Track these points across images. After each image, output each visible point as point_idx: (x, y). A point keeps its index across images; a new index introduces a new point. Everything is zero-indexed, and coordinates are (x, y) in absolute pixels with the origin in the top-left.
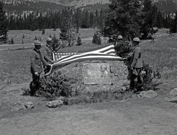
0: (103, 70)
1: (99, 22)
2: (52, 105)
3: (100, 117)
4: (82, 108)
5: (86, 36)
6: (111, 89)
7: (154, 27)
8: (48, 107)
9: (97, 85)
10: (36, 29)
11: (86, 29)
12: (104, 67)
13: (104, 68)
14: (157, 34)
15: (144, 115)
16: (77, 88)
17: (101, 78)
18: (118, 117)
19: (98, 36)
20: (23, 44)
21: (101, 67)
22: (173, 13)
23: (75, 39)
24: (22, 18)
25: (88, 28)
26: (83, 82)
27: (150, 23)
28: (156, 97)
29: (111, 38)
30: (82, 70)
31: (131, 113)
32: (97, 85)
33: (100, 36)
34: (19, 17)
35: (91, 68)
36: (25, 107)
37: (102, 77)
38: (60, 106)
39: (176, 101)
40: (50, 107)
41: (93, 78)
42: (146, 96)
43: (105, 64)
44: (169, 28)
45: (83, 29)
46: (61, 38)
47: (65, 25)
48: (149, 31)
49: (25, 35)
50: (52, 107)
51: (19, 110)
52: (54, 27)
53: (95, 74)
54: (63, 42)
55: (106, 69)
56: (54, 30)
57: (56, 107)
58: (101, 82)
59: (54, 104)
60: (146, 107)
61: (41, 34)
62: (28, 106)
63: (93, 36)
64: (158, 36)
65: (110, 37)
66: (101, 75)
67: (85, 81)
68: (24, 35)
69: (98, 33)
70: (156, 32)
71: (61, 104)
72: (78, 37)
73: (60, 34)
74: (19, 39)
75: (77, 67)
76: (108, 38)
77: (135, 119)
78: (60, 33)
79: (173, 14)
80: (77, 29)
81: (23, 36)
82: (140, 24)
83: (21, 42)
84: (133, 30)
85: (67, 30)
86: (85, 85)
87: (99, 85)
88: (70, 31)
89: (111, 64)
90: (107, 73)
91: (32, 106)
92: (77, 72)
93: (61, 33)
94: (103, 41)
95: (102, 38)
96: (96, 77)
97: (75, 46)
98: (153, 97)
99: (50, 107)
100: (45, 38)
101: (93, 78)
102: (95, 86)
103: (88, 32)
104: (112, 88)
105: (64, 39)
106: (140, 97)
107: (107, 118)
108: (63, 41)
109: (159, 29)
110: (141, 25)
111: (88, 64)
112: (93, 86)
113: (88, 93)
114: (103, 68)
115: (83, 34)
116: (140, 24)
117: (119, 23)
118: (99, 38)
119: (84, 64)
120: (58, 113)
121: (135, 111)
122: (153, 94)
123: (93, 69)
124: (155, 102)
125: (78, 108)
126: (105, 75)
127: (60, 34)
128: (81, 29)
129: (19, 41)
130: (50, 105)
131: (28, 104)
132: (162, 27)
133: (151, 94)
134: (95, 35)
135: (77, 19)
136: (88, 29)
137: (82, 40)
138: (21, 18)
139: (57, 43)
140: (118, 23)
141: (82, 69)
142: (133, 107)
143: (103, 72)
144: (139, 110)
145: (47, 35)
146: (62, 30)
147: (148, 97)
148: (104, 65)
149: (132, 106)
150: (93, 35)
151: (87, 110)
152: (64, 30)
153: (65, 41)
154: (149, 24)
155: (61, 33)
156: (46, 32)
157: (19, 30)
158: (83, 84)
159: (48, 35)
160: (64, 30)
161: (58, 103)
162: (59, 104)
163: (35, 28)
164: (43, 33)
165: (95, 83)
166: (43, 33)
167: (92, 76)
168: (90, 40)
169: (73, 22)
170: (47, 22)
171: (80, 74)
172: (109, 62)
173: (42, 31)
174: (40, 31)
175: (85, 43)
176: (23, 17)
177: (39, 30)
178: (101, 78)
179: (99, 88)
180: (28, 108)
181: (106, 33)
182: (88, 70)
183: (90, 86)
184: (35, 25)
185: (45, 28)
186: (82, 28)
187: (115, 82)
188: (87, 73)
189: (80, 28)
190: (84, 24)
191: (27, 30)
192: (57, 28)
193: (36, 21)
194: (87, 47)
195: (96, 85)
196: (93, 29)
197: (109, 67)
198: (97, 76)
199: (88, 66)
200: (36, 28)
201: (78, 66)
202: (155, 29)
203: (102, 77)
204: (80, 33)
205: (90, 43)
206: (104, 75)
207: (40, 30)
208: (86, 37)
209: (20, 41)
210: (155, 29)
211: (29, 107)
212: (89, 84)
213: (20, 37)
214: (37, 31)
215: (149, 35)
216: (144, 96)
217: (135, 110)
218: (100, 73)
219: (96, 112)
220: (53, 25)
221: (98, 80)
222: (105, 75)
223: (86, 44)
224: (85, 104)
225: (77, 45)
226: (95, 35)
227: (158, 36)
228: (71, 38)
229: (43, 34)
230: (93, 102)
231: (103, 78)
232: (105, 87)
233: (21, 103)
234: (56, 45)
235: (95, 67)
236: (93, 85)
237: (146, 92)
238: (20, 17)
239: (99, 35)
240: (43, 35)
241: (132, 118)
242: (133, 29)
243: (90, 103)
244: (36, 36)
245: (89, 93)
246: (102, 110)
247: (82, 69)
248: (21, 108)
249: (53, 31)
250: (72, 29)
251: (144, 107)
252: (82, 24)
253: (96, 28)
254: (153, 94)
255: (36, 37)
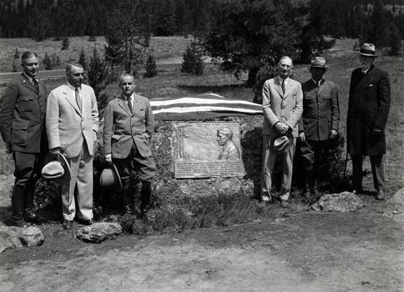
0: (223, 141)
1: (197, 21)
2: (92, 236)
3: (223, 270)
4: (173, 244)
5: (165, 53)
6: (245, 189)
7: (326, 35)
8: (81, 242)
9: (209, 178)
10: (48, 36)
11: (167, 38)
12: (225, 133)
13: (227, 135)
14: (331, 50)
15: (340, 262)
16: (158, 187)
17: (218, 161)
18: (271, 270)
19: (196, 54)
20: (15, 71)
21: (218, 131)
22: (366, 4)
23: (142, 62)
24: (14, 9)
25: (172, 34)
26: (173, 171)
27: (317, 26)
28: (361, 211)
29: (229, 60)
30: (169, 140)
31: (306, 257)
32: (209, 180)
33: (201, 55)
34: (6, 7)
35: (191, 135)
36: (19, 241)
37: (220, 157)
38: (114, 236)
39: (4, 37)
40: (86, 241)
41: (198, 161)
42: (335, 208)
43: (230, 124)
44: (358, 37)
45: (160, 37)
46: (107, 59)
47: (118, 28)
48: (313, 43)
49: (19, 50)
50: (95, 240)
51: (4, 251)
52: (91, 33)
53: (204, 151)
54: (113, 69)
55: (230, 137)
56: (90, 40)
57: (104, 240)
58: (217, 172)
59: (99, 234)
60: (342, 238)
61: (59, 50)
62: (30, 239)
63: (184, 56)
64: (334, 55)
65: (226, 57)
66: (219, 154)
67: (177, 169)
68: (17, 50)
69: (196, 47)
70: (330, 48)
71: (116, 232)
72: (147, 58)
73: (106, 48)
74: (5, 61)
75: (157, 134)
76: (221, 60)
77: (321, 275)
78: (105, 46)
79: (366, 6)
80: (147, 38)
81: (14, 54)
82: (297, 26)
83: (10, 67)
84: (282, 42)
85: (123, 41)
86: (179, 181)
87: (214, 179)
88: (129, 42)
89: (243, 125)
90: (233, 147)
91: (39, 238)
92: (157, 147)
93: (107, 45)
94: (206, 67)
95: (208, 60)
96: (206, 157)
97: (141, 77)
98: (352, 210)
99: (86, 241)
100: (68, 59)
101: (198, 161)
102: (204, 183)
103: (171, 45)
104: (247, 187)
105: (115, 62)
106: (318, 210)
107: (244, 273)
108: (112, 66)
109: (337, 40)
110: (299, 30)
111: (184, 124)
112: (197, 181)
113: (184, 199)
114: (224, 136)
115: (159, 51)
116: (297, 26)
117: (248, 23)
118: (199, 59)
119: (176, 126)
120: (115, 257)
121: (315, 251)
122: (353, 203)
123: (197, 138)
124: (362, 223)
125: (162, 245)
126: (229, 152)
127: (106, 48)
128: (155, 40)
129: (5, 66)
130: (87, 237)
131: (29, 234)
132: (342, 35)
133: (346, 203)
134: (187, 51)
135: (147, 15)
136: (171, 37)
137: (157, 63)
138: (12, 9)
139: (100, 71)
140: (246, 23)
141: (169, 138)
142: (306, 239)
143: (223, 145)
144: (325, 247)
145: (74, 51)
146: (110, 39)
147: (339, 209)
148: (225, 128)
149: (304, 237)
150: (183, 51)
151: (185, 248)
152: (114, 41)
153: (116, 65)
154: (313, 28)
155: (107, 45)
156: (71, 44)
157: (6, 39)
158: (173, 178)
159: (77, 50)
160: (114, 41)
161: (108, 231)
162: (111, 233)
163: (44, 34)
164: (65, 47)
165: (202, 174)
166: (65, 47)
167: (194, 156)
168: (177, 63)
169: (137, 22)
170: (74, 20)
171: (164, 152)
172: (239, 120)
173: (61, 42)
174: (56, 42)
175: (166, 71)
176: (16, 8)
177: (55, 40)
178: (218, 161)
179: (214, 188)
180: (29, 245)
181: (216, 48)
182: (185, 140)
183: (190, 181)
184: (45, 27)
185: (69, 36)
186: (157, 36)
187: (255, 171)
188: (182, 148)
189: (152, 34)
190: (162, 27)
191: (25, 40)
192: (98, 35)
193: (48, 18)
194: (170, 80)
195: (205, 180)
196: (182, 38)
197: (238, 132)
198: (209, 155)
199: (185, 129)
200: (46, 35)
201: (159, 130)
202: (328, 39)
203: (220, 157)
204: (153, 47)
205: (176, 70)
206: (225, 153)
207: (58, 40)
208: (166, 57)
209: (8, 65)
210: (328, 39)
211: (32, 241)
212: (188, 177)
213: (7, 56)
214: (50, 42)
215: (313, 52)
216: (331, 207)
217: (315, 248)
218: (215, 149)
219: (214, 255)
220: (88, 27)
221: (210, 165)
222: (229, 152)
223: (166, 73)
224: (179, 232)
225: (146, 76)
226: (188, 51)
227: (334, 55)
228: (131, 58)
229: (63, 49)
230: (201, 227)
231: (223, 160)
232: (227, 184)
233: (9, 233)
234: (98, 77)
235: (204, 133)
236: (198, 179)
237: (333, 196)
238: (10, 7)
239: (198, 52)
240: (63, 52)
241: (311, 272)
242: (281, 37)
243: (193, 228)
244: (46, 53)
245: (186, 199)
246: (228, 249)
247: (169, 138)
248: (10, 245)
249: (88, 43)
250: (135, 37)
251: (335, 239)
252: (158, 26)
253: (190, 36)
254: (353, 203)
255: (46, 57)
